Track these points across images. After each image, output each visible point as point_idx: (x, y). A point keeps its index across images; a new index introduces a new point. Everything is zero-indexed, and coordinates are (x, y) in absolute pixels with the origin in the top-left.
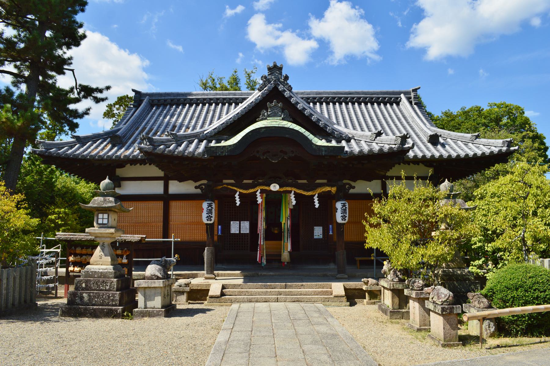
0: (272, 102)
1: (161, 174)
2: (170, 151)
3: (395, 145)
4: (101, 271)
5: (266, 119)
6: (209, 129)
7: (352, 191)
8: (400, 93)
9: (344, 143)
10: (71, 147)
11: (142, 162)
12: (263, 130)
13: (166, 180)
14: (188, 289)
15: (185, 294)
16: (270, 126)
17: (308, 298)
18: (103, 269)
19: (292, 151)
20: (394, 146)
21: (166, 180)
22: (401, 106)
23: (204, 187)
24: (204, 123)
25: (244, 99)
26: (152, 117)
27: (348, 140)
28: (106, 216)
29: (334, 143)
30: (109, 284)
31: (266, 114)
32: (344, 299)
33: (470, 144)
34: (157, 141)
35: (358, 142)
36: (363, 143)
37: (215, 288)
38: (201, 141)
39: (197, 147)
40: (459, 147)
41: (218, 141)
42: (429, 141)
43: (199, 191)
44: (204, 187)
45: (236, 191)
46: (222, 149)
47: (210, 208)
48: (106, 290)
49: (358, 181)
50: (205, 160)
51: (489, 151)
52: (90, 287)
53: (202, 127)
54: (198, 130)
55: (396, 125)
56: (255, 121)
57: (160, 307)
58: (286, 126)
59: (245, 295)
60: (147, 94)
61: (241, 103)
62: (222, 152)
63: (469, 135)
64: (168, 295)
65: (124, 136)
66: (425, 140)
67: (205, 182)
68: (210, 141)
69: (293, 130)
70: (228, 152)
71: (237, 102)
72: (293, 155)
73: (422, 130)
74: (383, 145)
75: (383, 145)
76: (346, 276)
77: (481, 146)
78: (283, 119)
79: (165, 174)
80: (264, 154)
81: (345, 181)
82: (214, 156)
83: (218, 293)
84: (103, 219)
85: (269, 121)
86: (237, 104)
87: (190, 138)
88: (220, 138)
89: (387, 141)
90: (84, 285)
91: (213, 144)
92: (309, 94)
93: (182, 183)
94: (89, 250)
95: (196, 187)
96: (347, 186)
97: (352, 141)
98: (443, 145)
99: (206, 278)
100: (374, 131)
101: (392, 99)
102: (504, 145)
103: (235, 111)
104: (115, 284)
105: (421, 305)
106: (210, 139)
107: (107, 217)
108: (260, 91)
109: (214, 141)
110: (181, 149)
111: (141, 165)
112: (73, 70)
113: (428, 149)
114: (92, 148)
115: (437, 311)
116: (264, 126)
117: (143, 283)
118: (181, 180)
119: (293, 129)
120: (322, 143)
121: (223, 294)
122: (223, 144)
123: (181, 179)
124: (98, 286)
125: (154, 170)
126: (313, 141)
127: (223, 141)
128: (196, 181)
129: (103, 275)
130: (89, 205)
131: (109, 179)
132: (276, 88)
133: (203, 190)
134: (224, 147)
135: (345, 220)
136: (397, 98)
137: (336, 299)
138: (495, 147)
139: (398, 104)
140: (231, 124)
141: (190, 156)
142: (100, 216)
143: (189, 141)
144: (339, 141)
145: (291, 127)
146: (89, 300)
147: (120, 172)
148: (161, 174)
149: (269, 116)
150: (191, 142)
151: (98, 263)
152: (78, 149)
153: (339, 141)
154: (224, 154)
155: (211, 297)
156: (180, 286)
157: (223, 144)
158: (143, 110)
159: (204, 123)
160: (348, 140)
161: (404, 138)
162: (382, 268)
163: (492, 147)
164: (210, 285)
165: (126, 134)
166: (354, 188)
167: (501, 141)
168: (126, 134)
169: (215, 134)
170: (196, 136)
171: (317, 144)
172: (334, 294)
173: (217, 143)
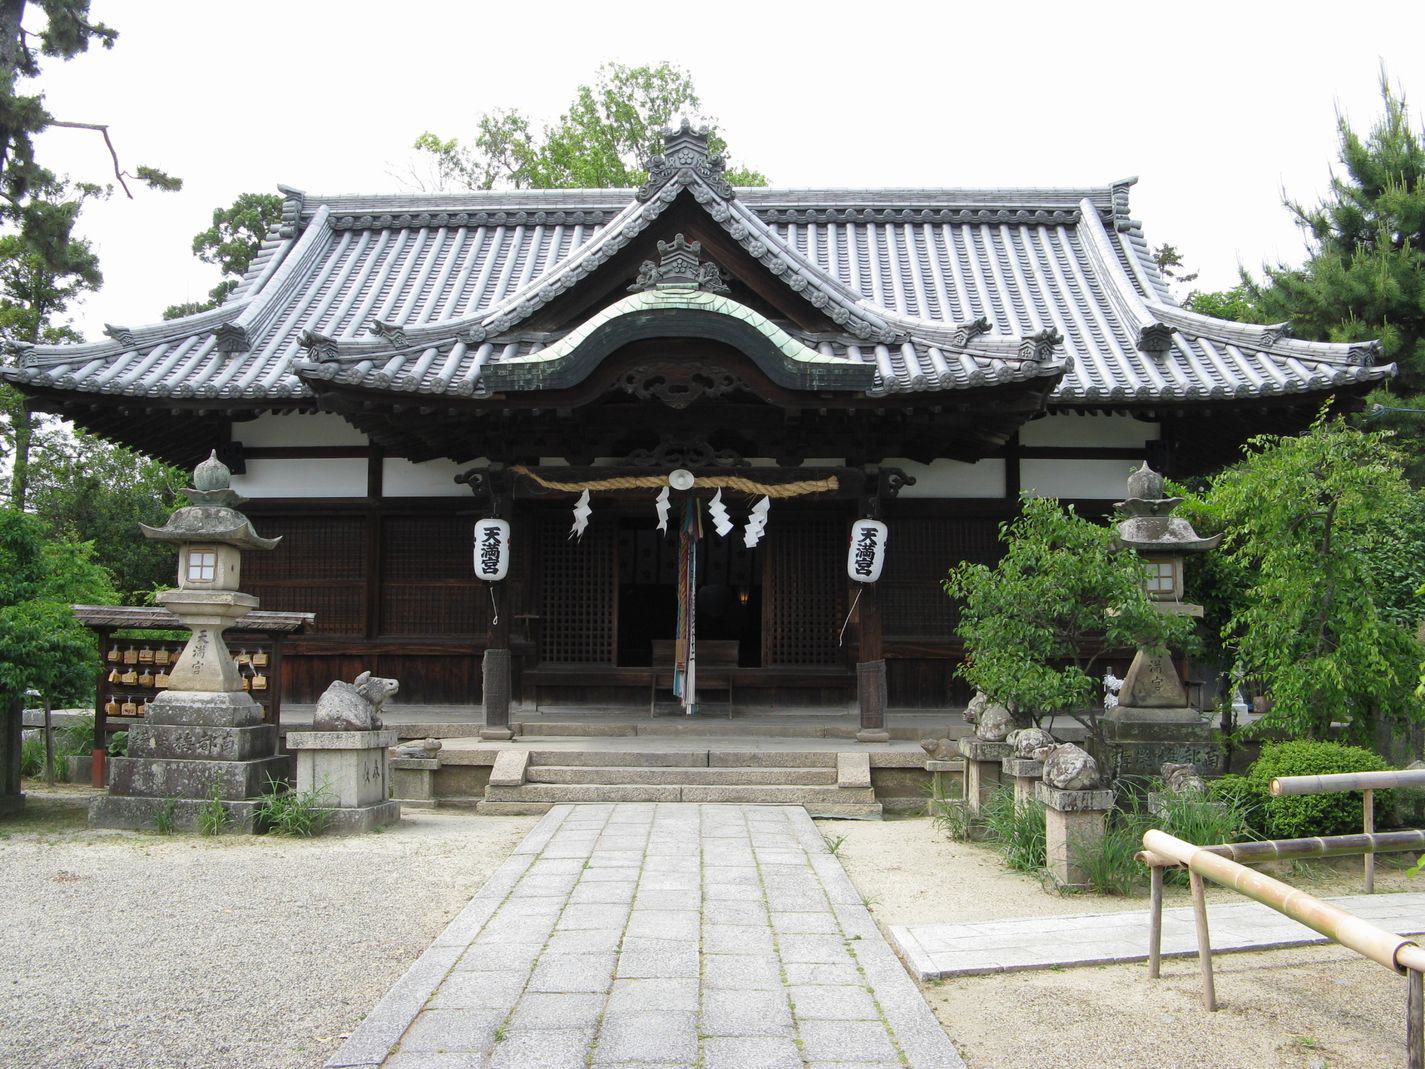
0: (669, 240)
1: (362, 440)
2: (383, 378)
3: (1022, 361)
4: (197, 705)
5: (653, 286)
6: (499, 308)
7: (906, 492)
8: (1078, 196)
9: (881, 355)
10: (108, 360)
11: (304, 405)
12: (644, 319)
13: (375, 458)
14: (434, 764)
15: (426, 777)
16: (663, 306)
17: (766, 792)
18: (202, 702)
19: (727, 378)
20: (1017, 365)
21: (375, 458)
22: (1081, 238)
23: (479, 477)
24: (488, 288)
25: (609, 214)
26: (336, 267)
27: (894, 348)
28: (209, 559)
29: (854, 358)
30: (219, 741)
31: (654, 273)
32: (870, 794)
33: (1261, 356)
34: (349, 348)
35: (921, 351)
36: (934, 353)
37: (509, 760)
38: (473, 347)
39: (460, 367)
40: (1230, 363)
41: (523, 347)
42: (1142, 346)
43: (465, 490)
44: (479, 477)
45: (577, 496)
46: (529, 371)
47: (492, 541)
48: (210, 757)
49: (938, 461)
50: (481, 403)
51: (1283, 380)
52: (170, 748)
53: (483, 301)
54: (469, 314)
55: (1056, 294)
56: (620, 293)
57: (355, 802)
58: (707, 308)
59: (591, 782)
60: (321, 202)
61: (603, 224)
62: (528, 382)
63: (1259, 329)
64: (376, 774)
65: (255, 330)
66: (1132, 339)
67: (482, 462)
68: (498, 348)
69: (728, 318)
70: (544, 380)
71: (590, 221)
72: (729, 389)
73: (1127, 312)
74: (988, 361)
75: (988, 361)
76: (885, 735)
77: (1291, 362)
78: (701, 287)
79: (371, 441)
80: (648, 385)
81: (889, 463)
82: (506, 393)
83: (516, 775)
84: (202, 566)
85: (660, 294)
86: (588, 227)
87: (442, 342)
88: (527, 337)
89: (998, 351)
90: (152, 743)
91: (506, 358)
92: (805, 199)
93: (421, 466)
94: (162, 656)
95: (459, 480)
96: (892, 478)
97: (907, 349)
98: (1183, 360)
99: (487, 738)
100: (969, 318)
101: (1052, 217)
102: (1354, 360)
103: (580, 252)
104: (236, 740)
105: (245, 504)
106: (500, 340)
107: (213, 563)
108: (644, 202)
109: (508, 350)
110: (418, 368)
111: (302, 412)
112: (103, 129)
113: (1136, 367)
114: (167, 363)
115: (1053, 805)
116: (645, 307)
117: (309, 740)
118: (417, 457)
119: (728, 317)
120: (825, 357)
121: (527, 779)
122: (536, 356)
123: (418, 454)
124: (191, 746)
125: (338, 430)
126: (786, 351)
127: (533, 350)
128: (460, 458)
129: (203, 718)
130: (164, 530)
131: (219, 457)
132: (685, 197)
133: (478, 486)
134: (535, 365)
135: (868, 573)
136: (1069, 212)
137: (846, 793)
138: (1330, 364)
139: (1071, 227)
140: (557, 299)
141: (440, 390)
142: (195, 559)
143: (437, 348)
144: (867, 349)
145: (724, 311)
146: (166, 782)
147: (243, 433)
148: (362, 440)
149: (661, 278)
150: (443, 351)
151: (189, 684)
152: (127, 368)
153: (867, 349)
154: (533, 388)
155: (497, 786)
156: (411, 755)
157: (536, 356)
158: (311, 250)
159: (488, 288)
160: (894, 348)
161: (1049, 341)
162: (966, 705)
163: (1322, 367)
164: (495, 754)
165: (261, 322)
166: (911, 482)
167: (1345, 347)
168: (261, 322)
169: (512, 329)
170: (460, 332)
171: (796, 358)
172: (841, 780)
173: (516, 354)
